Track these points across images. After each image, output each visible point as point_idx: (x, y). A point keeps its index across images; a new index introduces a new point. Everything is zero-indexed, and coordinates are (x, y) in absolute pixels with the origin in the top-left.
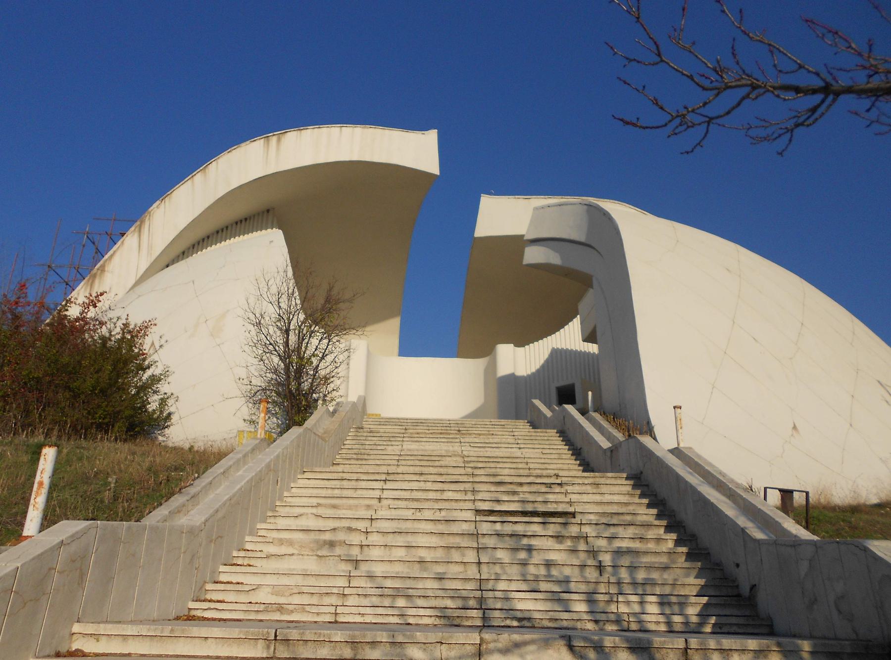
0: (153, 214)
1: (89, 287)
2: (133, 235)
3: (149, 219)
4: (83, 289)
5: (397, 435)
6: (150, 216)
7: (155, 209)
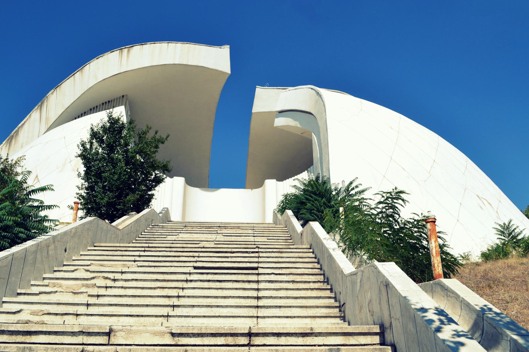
0: (49, 97)
1: (8, 145)
2: (37, 111)
3: (47, 101)
4: (5, 146)
5: (178, 229)
6: (47, 99)
7: (51, 95)
